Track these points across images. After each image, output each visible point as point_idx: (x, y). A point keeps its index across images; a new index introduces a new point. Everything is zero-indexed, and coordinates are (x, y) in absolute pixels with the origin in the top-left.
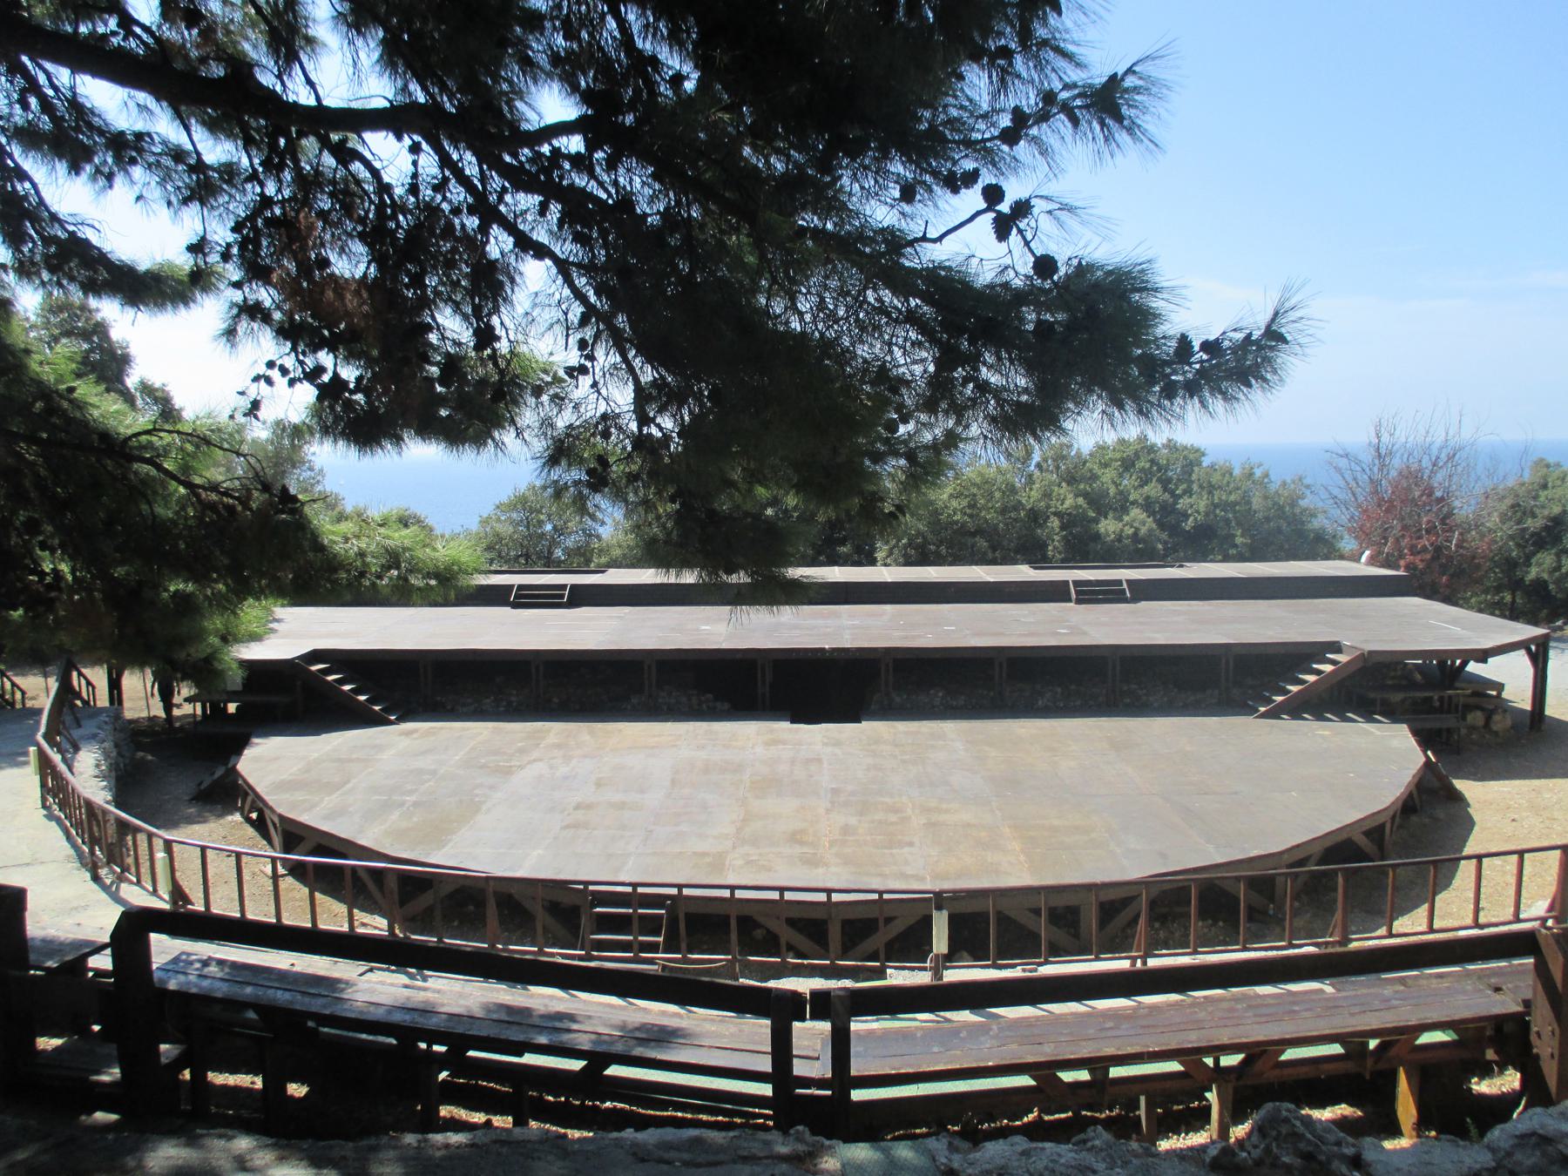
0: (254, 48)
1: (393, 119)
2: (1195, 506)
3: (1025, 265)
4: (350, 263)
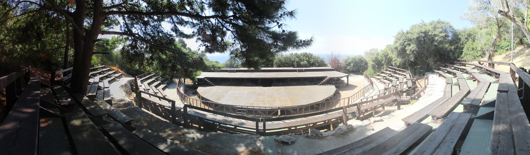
0: (199, 11)
1: (213, 17)
2: (312, 61)
3: (281, 31)
4: (209, 33)
